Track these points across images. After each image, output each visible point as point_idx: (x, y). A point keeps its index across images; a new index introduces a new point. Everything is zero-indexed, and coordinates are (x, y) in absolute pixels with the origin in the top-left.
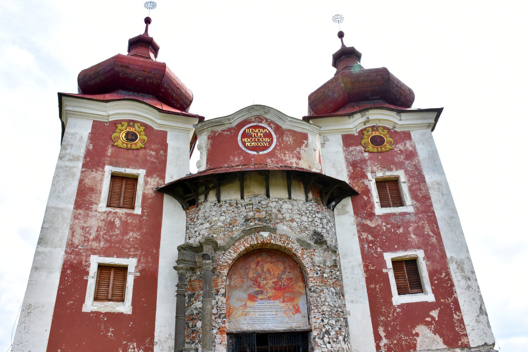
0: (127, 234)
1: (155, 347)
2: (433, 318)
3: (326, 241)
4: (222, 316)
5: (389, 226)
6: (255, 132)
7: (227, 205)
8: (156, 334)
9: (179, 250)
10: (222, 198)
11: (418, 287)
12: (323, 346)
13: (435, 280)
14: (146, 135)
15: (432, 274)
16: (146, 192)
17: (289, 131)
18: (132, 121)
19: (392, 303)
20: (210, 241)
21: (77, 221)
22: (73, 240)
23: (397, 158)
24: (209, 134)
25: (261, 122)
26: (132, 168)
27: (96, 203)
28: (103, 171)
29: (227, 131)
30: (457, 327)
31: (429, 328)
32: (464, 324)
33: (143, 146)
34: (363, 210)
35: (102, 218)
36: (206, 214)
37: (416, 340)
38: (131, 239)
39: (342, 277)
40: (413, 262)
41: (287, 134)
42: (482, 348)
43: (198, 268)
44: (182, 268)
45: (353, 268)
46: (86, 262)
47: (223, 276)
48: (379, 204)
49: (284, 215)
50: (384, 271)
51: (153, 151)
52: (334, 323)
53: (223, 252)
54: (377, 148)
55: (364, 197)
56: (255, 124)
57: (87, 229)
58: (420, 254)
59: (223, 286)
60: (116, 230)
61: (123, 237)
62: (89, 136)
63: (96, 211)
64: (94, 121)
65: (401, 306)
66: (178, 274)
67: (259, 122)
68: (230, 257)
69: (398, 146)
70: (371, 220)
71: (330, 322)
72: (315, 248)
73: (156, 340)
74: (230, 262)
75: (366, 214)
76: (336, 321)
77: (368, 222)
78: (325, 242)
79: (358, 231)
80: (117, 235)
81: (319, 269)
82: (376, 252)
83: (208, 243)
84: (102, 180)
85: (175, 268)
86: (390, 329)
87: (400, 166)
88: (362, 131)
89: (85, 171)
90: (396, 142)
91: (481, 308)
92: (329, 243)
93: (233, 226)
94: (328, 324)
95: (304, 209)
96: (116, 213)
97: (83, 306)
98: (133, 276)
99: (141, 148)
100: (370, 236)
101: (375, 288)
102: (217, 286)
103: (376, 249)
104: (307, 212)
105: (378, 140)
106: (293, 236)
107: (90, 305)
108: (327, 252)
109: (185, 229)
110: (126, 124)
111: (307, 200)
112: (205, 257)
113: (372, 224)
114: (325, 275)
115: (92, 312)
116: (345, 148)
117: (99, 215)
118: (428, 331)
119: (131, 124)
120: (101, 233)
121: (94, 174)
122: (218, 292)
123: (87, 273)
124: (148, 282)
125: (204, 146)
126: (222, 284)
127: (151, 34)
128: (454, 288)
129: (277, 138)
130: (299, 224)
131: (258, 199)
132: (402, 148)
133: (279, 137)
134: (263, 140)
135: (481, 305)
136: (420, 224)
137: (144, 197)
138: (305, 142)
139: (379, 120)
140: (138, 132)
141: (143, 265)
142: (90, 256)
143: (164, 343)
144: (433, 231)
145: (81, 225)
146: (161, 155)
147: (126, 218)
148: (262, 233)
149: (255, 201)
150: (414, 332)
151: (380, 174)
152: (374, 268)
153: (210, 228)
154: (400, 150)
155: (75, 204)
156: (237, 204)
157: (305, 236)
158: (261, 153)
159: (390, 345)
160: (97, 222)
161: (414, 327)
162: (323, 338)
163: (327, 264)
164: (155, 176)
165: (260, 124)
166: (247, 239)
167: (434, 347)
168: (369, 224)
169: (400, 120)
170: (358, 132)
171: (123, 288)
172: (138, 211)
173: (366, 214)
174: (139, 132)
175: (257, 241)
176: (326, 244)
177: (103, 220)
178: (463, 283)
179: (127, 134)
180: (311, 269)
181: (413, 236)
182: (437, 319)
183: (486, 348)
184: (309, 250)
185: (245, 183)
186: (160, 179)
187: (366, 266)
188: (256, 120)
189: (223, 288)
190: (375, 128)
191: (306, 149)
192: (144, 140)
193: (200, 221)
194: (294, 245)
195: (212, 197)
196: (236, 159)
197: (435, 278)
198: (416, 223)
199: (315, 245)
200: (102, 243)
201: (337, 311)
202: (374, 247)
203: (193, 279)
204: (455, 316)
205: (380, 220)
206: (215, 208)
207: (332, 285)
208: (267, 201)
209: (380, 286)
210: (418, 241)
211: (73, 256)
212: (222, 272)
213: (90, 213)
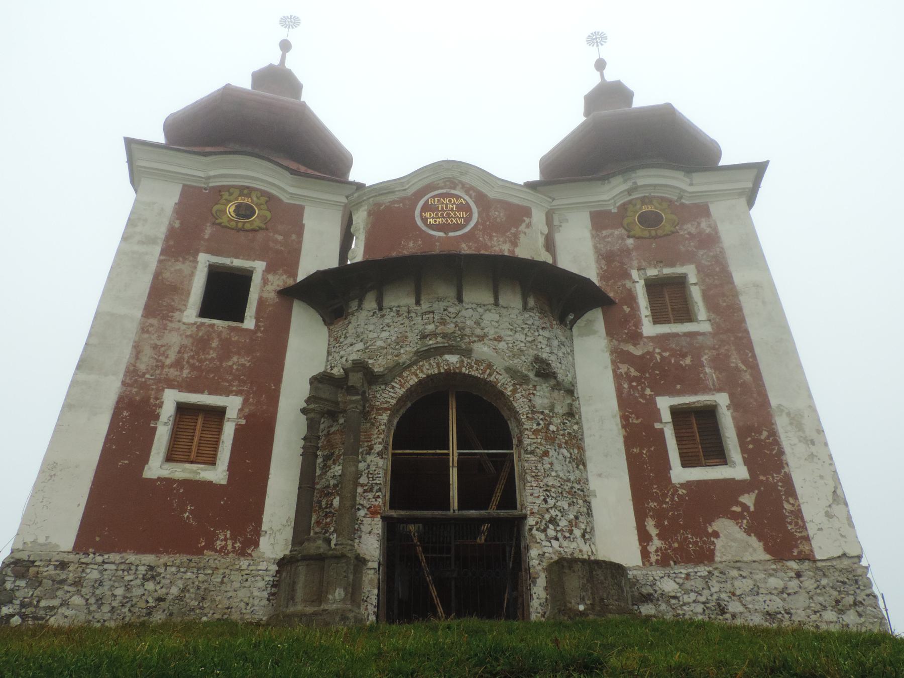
0: (229, 358)
1: (262, 539)
2: (745, 507)
3: (554, 373)
4: (376, 488)
5: (666, 354)
7: (392, 314)
8: (266, 518)
9: (311, 383)
10: (386, 303)
11: (718, 455)
12: (544, 543)
13: (750, 443)
14: (269, 210)
15: (743, 433)
16: (265, 295)
18: (248, 187)
19: (670, 479)
20: (360, 366)
21: (146, 336)
22: (137, 365)
25: (454, 188)
28: (195, 261)
30: (790, 523)
31: (737, 524)
32: (802, 518)
33: (264, 226)
34: (622, 328)
35: (189, 333)
36: (359, 330)
37: (713, 543)
38: (235, 367)
39: (582, 435)
40: (709, 414)
42: (838, 562)
43: (341, 412)
44: (313, 410)
46: (156, 399)
48: (651, 319)
49: (486, 330)
50: (657, 426)
52: (566, 507)
53: (383, 387)
55: (625, 307)
56: (444, 191)
57: (163, 349)
58: (722, 400)
59: (380, 440)
60: (211, 352)
61: (221, 364)
62: (175, 208)
63: (179, 321)
65: (688, 485)
66: (307, 419)
67: (451, 188)
68: (393, 395)
69: (685, 227)
70: (635, 345)
71: (559, 504)
73: (264, 527)
74: (394, 402)
75: (627, 334)
76: (570, 505)
77: (631, 348)
78: (553, 375)
79: (613, 362)
81: (541, 417)
82: (643, 396)
84: (192, 275)
85: (304, 411)
86: (666, 523)
88: (624, 205)
91: (835, 492)
92: (560, 377)
94: (555, 506)
95: (520, 322)
96: (213, 326)
97: (146, 468)
99: (261, 229)
100: (632, 370)
101: (641, 453)
102: (369, 439)
103: (643, 390)
104: (524, 326)
106: (499, 364)
107: (156, 467)
108: (556, 391)
109: (326, 354)
110: (237, 192)
111: (525, 308)
112: (351, 390)
113: (637, 352)
115: (159, 479)
116: (594, 232)
117: (183, 327)
118: (737, 528)
119: (245, 192)
120: (186, 356)
121: (179, 266)
123: (157, 417)
124: (256, 437)
125: (362, 227)
127: (288, 65)
128: (784, 458)
129: (479, 213)
130: (510, 345)
131: (443, 305)
132: (693, 230)
135: (836, 488)
136: (722, 351)
137: (261, 302)
138: (527, 220)
140: (257, 205)
141: (252, 408)
142: (163, 390)
143: (278, 533)
144: (745, 362)
145: (152, 342)
147: (229, 334)
148: (447, 357)
149: (439, 307)
150: (710, 530)
151: (652, 272)
152: (639, 421)
153: (364, 351)
154: (689, 233)
156: (409, 312)
157: (522, 364)
158: (451, 234)
159: (666, 549)
161: (710, 521)
162: (544, 530)
163: (556, 410)
164: (280, 272)
165: (453, 192)
167: (747, 557)
169: (691, 184)
170: (618, 208)
171: (215, 444)
172: (249, 323)
174: (258, 205)
175: (439, 369)
176: (555, 378)
177: (191, 336)
178: (801, 449)
179: (238, 207)
181: (708, 370)
182: (752, 509)
183: (846, 563)
184: (525, 387)
186: (289, 277)
187: (625, 418)
189: (380, 443)
190: (647, 200)
191: (527, 230)
193: (349, 340)
194: (501, 377)
195: (370, 304)
196: (411, 244)
197: (749, 439)
198: (714, 348)
199: (537, 379)
200: (186, 372)
201: (572, 488)
203: (333, 430)
204: (786, 505)
206: (374, 320)
207: (563, 445)
208: (458, 308)
209: (649, 451)
210: (718, 378)
211: (135, 390)
213: (169, 324)
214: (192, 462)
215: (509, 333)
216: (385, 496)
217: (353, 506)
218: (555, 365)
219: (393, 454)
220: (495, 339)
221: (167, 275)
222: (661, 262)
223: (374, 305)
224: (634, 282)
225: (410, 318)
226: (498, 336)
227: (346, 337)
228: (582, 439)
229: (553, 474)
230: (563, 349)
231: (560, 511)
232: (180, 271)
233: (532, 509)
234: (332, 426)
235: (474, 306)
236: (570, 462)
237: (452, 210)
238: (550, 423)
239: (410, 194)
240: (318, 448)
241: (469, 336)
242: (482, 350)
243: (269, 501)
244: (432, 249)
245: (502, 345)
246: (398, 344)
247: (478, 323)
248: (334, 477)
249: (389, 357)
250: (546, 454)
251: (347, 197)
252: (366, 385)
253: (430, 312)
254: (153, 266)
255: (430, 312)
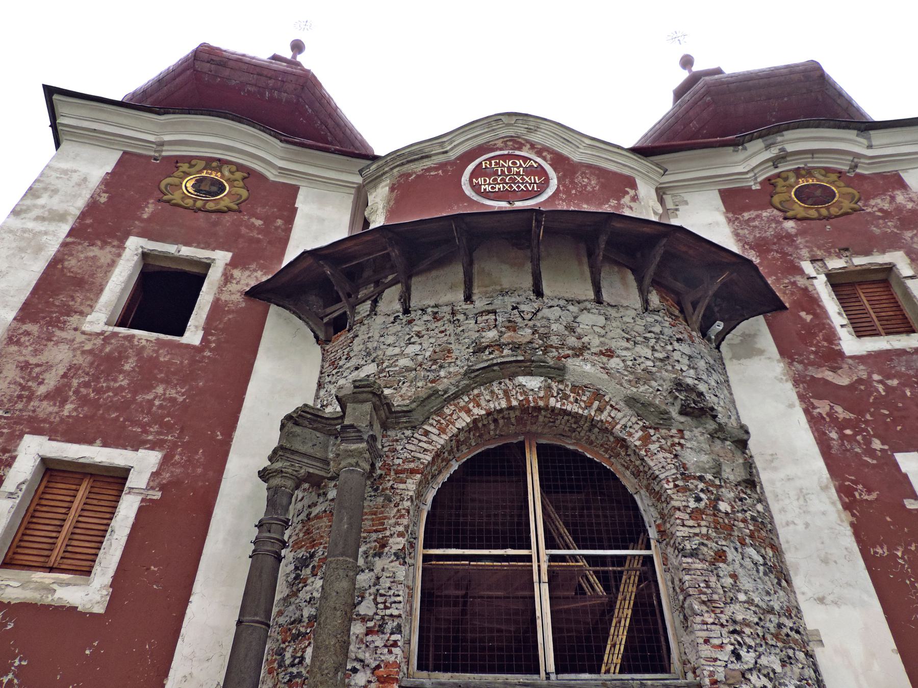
0: (149, 388)
4: (391, 625)
5: (894, 382)
6: (503, 166)
7: (425, 318)
16: (224, 297)
17: (589, 166)
18: (219, 160)
20: (365, 390)
23: (877, 226)
24: (395, 181)
25: (520, 149)
26: (196, 247)
27: (82, 313)
28: (122, 247)
29: (436, 169)
33: (236, 207)
34: (805, 346)
35: (88, 347)
36: (370, 345)
38: (157, 403)
39: (772, 522)
41: (584, 173)
45: (803, 495)
47: (402, 500)
48: (851, 329)
49: (585, 339)
51: (257, 218)
53: (408, 433)
54: (817, 210)
55: (803, 314)
56: (506, 152)
57: (37, 370)
59: (401, 529)
60: (121, 377)
63: (76, 329)
64: (125, 153)
70: (834, 370)
71: (764, 661)
72: (681, 427)
75: (815, 353)
76: (783, 663)
77: (829, 375)
79: (801, 397)
80: (122, 388)
81: (701, 486)
82: (871, 452)
83: (361, 397)
84: (112, 264)
85: (264, 475)
87: (891, 243)
88: (769, 179)
89: (73, 243)
90: (867, 197)
92: (722, 419)
93: (441, 367)
95: (640, 329)
98: (139, 498)
99: (230, 210)
100: (839, 409)
102: (380, 525)
103: (868, 442)
104: (649, 335)
105: (818, 193)
106: (614, 392)
108: (718, 442)
111: (646, 307)
113: (843, 380)
114: (724, 506)
116: (730, 215)
117: (80, 338)
120: (75, 382)
121: (95, 251)
122: (384, 546)
124: (181, 516)
125: (381, 207)
126: (397, 524)
129: (558, 178)
131: (510, 300)
132: (886, 206)
133: (564, 176)
134: (523, 179)
137: (217, 307)
139: (813, 152)
141: (178, 471)
142: (21, 437)
145: (22, 359)
146: (277, 228)
147: (157, 352)
148: (522, 380)
151: (836, 264)
152: (874, 496)
154: (881, 210)
155: (21, 309)
156: (453, 313)
160: (71, 354)
163: (725, 475)
164: (253, 266)
165: (517, 153)
166: (478, 395)
168: (830, 379)
169: (870, 147)
170: (761, 183)
172: (193, 336)
173: (815, 353)
175: (508, 400)
176: (714, 417)
177: (91, 352)
180: (676, 486)
185: (474, 254)
187: (845, 492)
188: (506, 146)
189: (401, 535)
191: (632, 204)
192: (241, 196)
193: (353, 362)
194: (620, 415)
195: (391, 301)
201: (780, 626)
202: (859, 438)
203: (315, 511)
205: (861, 367)
207: (748, 540)
212: (402, 486)
213: (58, 333)
214: (51, 570)
215: (625, 344)
216: (408, 642)
217: (340, 667)
218: (711, 399)
219: (426, 558)
220: (601, 353)
221: (71, 263)
222: (847, 250)
223: (397, 306)
224: (809, 278)
225: (455, 322)
226: (607, 349)
227: (348, 358)
228: (773, 531)
229: (742, 597)
230: (715, 376)
231: (766, 675)
232: (94, 258)
233: (712, 674)
234: (315, 504)
235: (562, 303)
236: (765, 574)
237: (518, 174)
238: (718, 499)
239: (453, 158)
240: (284, 544)
241: (557, 348)
242: (583, 369)
243: (182, 649)
244: (490, 222)
245: (614, 363)
246: (435, 362)
247: (571, 329)
248: (310, 601)
249: (420, 384)
250: (720, 556)
251: (361, 172)
252: (377, 426)
253: (489, 312)
254: (52, 248)
255: (489, 312)
